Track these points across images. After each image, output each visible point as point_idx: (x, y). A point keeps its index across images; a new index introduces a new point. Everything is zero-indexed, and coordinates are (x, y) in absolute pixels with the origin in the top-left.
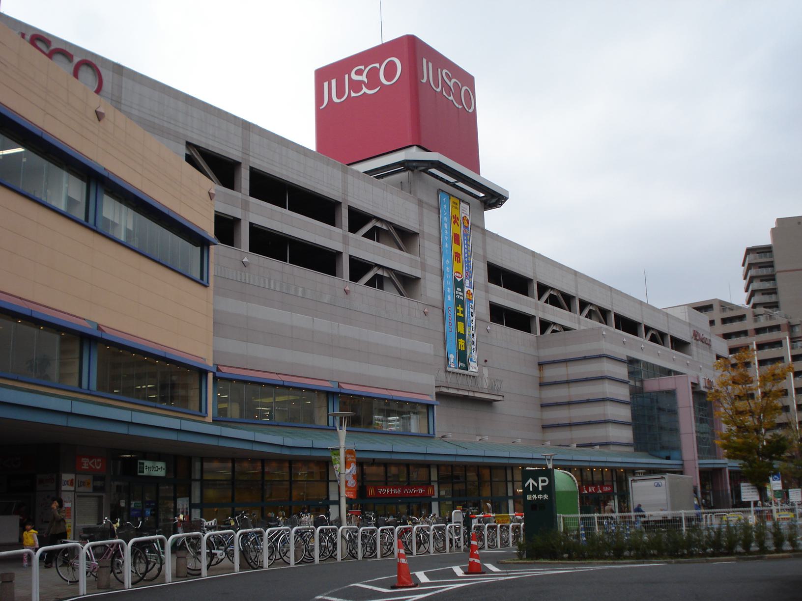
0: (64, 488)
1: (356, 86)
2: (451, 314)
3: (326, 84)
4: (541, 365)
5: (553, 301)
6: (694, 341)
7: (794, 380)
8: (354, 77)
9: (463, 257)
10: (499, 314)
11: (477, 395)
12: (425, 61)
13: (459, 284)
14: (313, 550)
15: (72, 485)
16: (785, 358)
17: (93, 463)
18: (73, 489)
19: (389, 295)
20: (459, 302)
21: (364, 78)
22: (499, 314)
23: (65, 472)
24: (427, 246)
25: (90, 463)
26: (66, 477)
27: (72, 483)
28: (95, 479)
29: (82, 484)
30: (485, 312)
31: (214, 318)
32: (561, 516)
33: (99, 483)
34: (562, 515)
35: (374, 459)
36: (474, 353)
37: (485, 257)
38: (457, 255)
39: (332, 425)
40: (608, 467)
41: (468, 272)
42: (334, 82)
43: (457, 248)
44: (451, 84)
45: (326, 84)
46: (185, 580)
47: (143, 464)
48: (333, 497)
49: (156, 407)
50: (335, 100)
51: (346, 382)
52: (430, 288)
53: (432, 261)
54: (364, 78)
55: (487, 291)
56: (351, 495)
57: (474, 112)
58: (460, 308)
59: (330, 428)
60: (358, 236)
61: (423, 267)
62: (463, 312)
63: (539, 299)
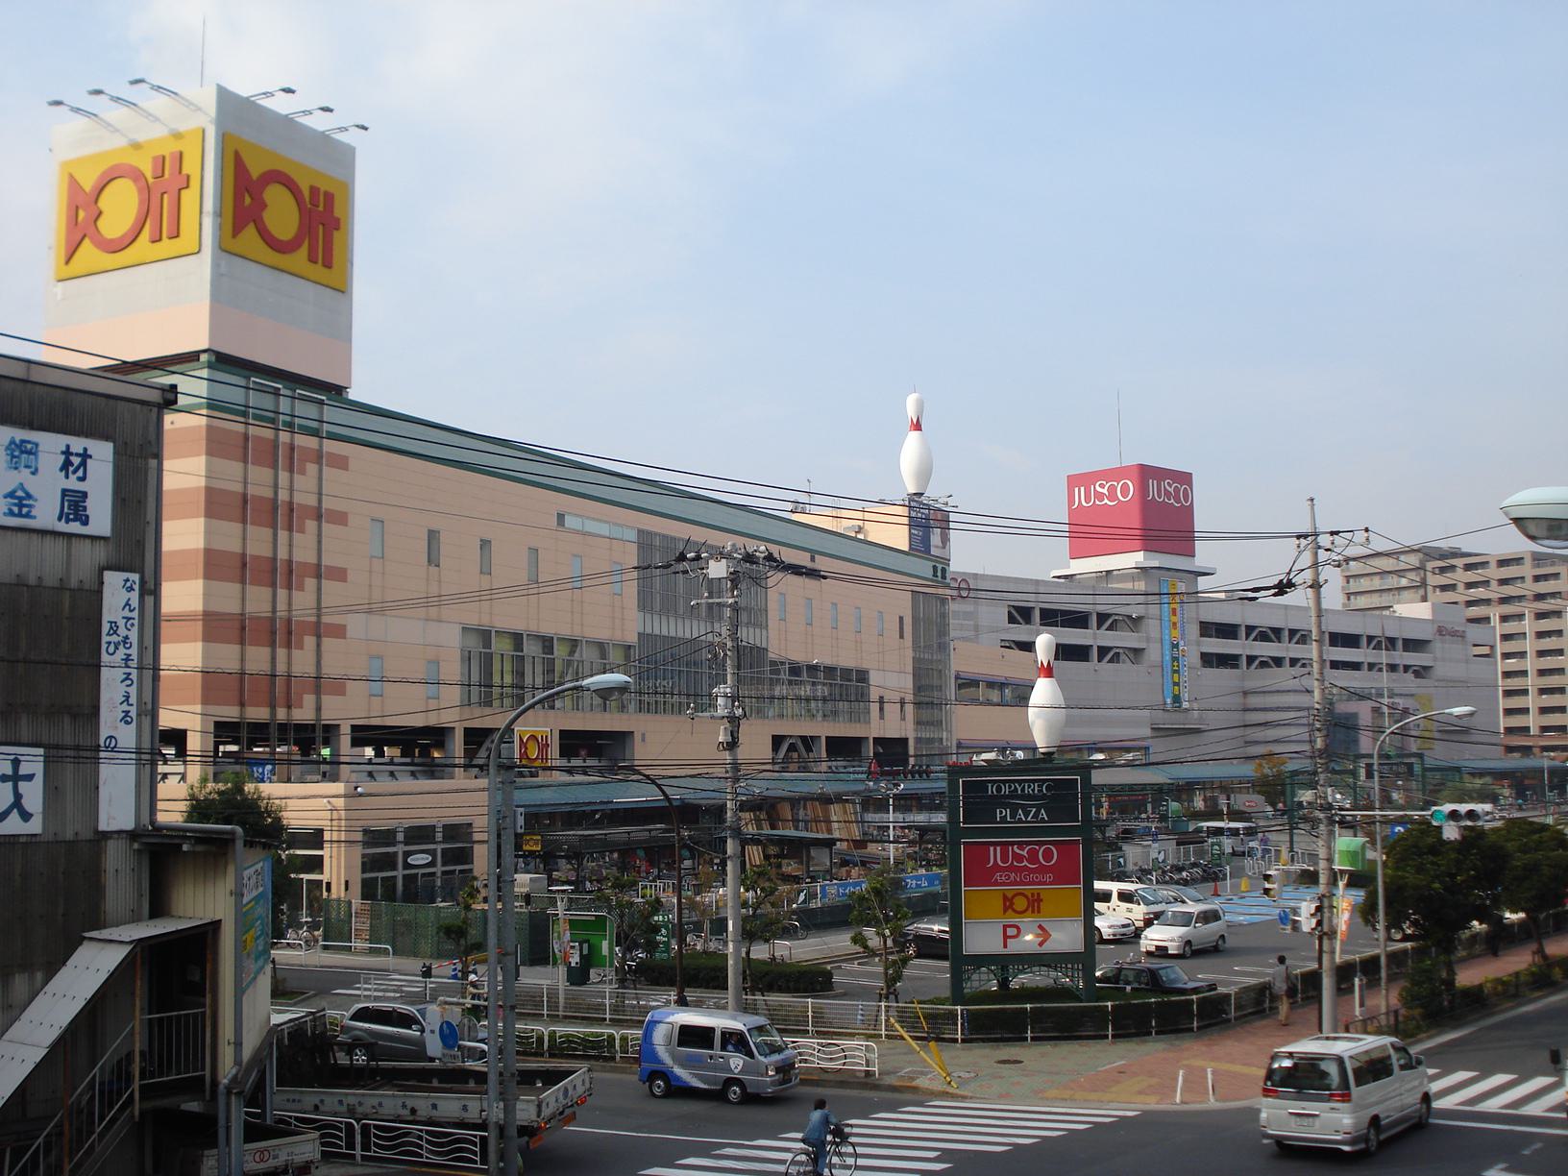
1: (1100, 496)
2: (1168, 669)
4: (1245, 693)
5: (1263, 637)
6: (1437, 637)
7: (1502, 663)
8: (1098, 489)
9: (1178, 625)
10: (1209, 660)
11: (1187, 726)
12: (1151, 481)
13: (1175, 646)
16: (1564, 632)
19: (1125, 667)
20: (1175, 659)
21: (1105, 491)
22: (1209, 660)
24: (1152, 627)
30: (1196, 660)
36: (1186, 695)
37: (1198, 618)
38: (1175, 624)
41: (1183, 635)
42: (1082, 489)
43: (1174, 619)
44: (1171, 490)
45: (1077, 489)
46: (938, 1009)
49: (228, 1128)
50: (1084, 504)
51: (176, 209)
52: (1153, 654)
53: (1155, 633)
54: (1105, 491)
55: (1198, 644)
57: (1191, 507)
58: (1176, 664)
60: (1102, 631)
61: (1148, 640)
62: (1178, 666)
63: (1246, 639)
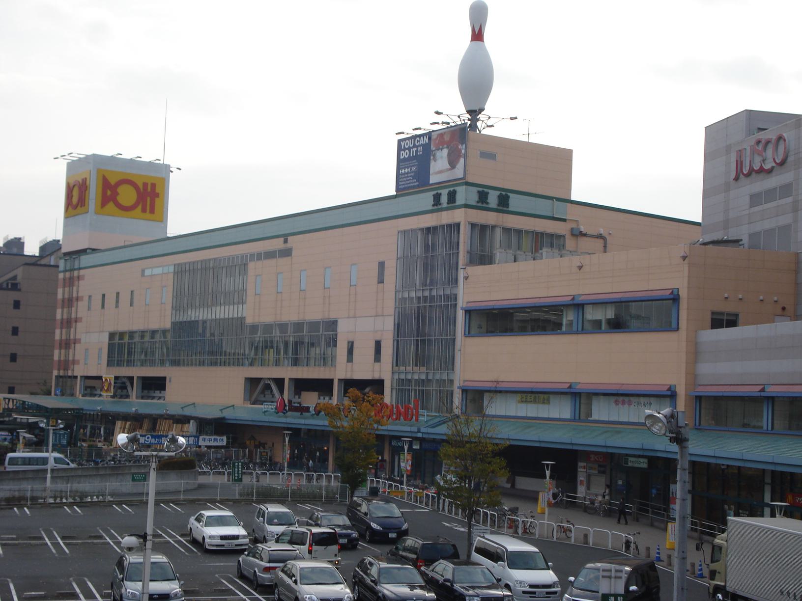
0: (579, 470)
3: (414, 154)
14: (141, 451)
15: (584, 468)
17: (598, 458)
18: (585, 470)
23: (581, 462)
25: (596, 458)
26: (580, 464)
27: (584, 468)
28: (600, 466)
29: (591, 468)
31: (336, 370)
32: (181, 483)
33: (602, 469)
34: (182, 481)
35: (434, 439)
39: (766, 429)
40: (648, 456)
45: (414, 154)
47: (628, 459)
48: (26, 421)
56: (18, 420)
59: (764, 432)
